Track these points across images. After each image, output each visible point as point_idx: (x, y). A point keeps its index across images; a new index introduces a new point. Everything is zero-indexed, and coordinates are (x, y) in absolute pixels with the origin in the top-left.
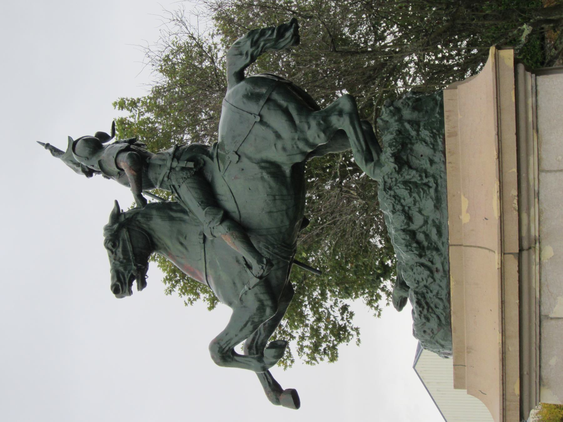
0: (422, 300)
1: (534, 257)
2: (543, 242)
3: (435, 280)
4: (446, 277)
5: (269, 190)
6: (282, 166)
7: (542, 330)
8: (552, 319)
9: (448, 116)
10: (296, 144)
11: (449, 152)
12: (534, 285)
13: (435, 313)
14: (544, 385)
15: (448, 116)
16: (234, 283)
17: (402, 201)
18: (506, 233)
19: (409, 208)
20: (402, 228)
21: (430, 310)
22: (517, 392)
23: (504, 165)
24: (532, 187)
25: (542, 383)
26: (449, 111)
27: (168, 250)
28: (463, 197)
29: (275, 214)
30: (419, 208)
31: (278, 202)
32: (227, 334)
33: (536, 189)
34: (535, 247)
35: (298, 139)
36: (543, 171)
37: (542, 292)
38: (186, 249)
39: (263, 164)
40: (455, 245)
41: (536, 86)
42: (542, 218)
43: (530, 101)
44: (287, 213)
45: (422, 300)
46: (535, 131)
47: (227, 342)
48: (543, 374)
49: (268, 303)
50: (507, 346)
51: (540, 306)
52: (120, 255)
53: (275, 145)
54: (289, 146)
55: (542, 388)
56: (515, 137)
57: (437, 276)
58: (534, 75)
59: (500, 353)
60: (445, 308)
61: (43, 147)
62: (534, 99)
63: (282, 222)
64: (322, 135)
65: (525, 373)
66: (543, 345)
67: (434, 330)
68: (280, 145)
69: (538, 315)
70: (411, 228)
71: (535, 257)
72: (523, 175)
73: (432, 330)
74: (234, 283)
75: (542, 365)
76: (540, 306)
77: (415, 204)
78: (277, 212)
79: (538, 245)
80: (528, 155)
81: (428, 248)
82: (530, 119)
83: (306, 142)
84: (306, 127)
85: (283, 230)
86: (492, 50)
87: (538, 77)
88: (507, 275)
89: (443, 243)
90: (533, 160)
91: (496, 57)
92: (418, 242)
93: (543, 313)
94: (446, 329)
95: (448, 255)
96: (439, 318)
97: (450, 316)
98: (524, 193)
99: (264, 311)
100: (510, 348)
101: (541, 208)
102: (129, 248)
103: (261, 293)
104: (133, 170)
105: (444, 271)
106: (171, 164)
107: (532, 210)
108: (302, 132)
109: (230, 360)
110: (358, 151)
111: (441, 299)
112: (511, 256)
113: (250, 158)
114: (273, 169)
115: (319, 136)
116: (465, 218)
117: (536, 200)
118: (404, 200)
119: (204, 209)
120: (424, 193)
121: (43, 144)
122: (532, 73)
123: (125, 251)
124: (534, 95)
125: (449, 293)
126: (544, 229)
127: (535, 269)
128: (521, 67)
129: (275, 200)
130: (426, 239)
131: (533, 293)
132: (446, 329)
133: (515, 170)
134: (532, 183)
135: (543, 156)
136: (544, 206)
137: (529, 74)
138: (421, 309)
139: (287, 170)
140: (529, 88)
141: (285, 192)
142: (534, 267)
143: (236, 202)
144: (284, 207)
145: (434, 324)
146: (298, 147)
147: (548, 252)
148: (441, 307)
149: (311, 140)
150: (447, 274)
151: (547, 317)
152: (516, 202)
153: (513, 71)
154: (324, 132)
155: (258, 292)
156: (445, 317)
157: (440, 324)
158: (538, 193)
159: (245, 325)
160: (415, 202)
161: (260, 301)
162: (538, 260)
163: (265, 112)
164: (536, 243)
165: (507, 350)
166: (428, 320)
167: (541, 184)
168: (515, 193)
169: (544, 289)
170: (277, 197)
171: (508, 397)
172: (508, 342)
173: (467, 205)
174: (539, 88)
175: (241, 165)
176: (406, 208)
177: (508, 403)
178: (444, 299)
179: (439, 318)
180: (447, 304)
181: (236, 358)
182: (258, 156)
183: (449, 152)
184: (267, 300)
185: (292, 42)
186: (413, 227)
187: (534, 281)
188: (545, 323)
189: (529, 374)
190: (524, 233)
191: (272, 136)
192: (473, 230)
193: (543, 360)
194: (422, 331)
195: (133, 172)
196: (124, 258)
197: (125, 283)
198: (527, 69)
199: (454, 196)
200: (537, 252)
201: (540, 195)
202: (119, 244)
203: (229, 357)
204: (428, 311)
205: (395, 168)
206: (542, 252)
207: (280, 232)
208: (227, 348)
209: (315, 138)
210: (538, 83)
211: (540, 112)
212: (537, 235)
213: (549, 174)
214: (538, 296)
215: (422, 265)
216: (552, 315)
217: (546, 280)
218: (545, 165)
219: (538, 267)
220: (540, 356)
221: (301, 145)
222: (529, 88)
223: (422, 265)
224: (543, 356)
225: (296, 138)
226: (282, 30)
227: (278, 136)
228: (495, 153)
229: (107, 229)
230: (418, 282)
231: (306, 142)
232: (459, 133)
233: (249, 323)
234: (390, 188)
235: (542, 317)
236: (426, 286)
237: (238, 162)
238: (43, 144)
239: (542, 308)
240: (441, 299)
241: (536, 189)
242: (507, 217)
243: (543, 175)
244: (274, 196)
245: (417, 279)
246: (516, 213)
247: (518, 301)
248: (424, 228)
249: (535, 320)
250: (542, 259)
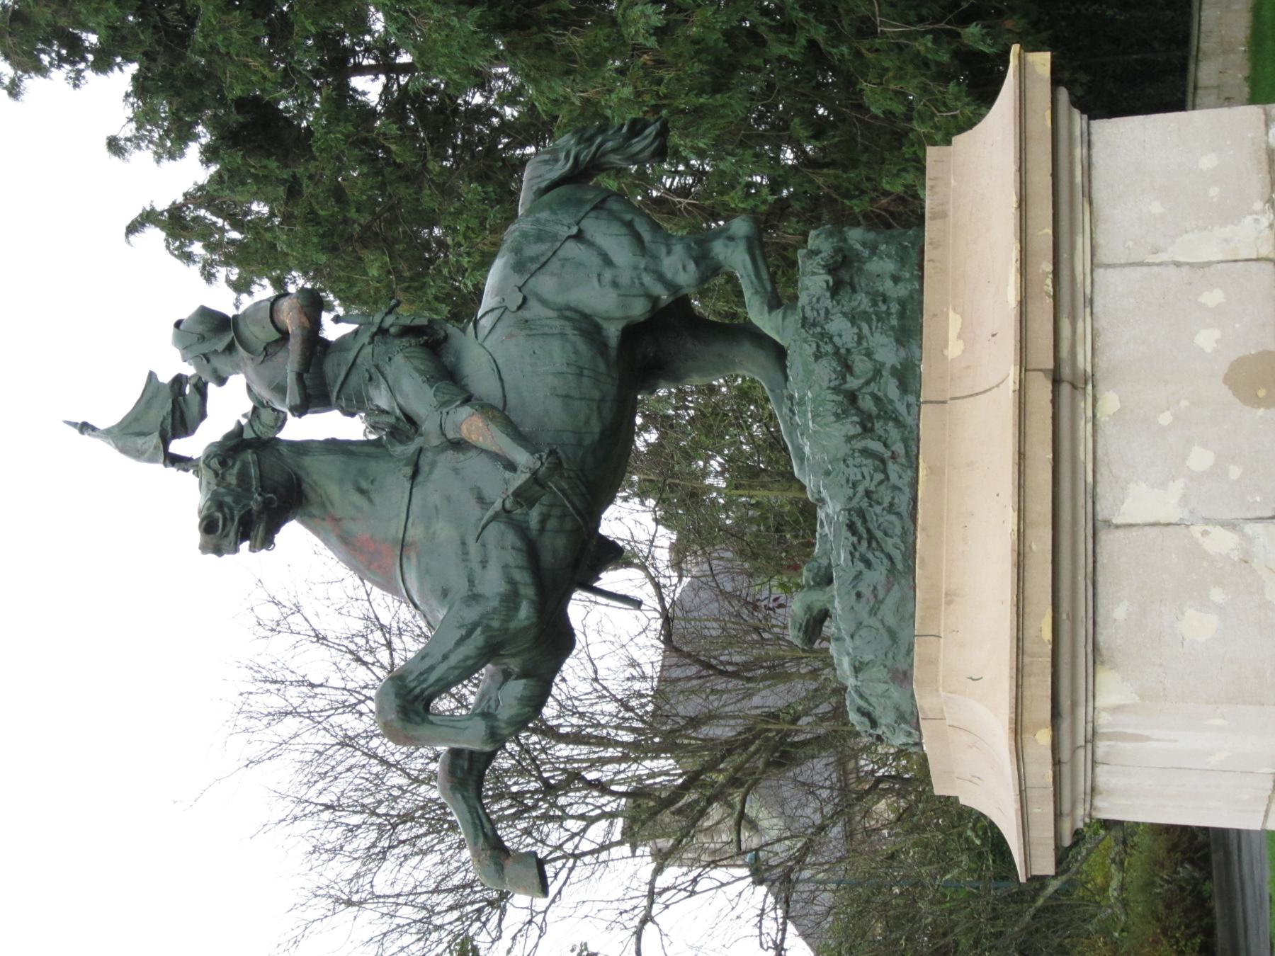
0: (859, 523)
1: (1082, 405)
2: (1100, 386)
3: (887, 478)
4: (911, 467)
5: (573, 357)
6: (605, 325)
7: (1098, 550)
8: (1117, 527)
9: (932, 187)
10: (640, 279)
11: (931, 244)
12: (1082, 457)
13: (882, 551)
14: (1102, 663)
15: (932, 187)
16: (464, 543)
17: (836, 339)
18: (1031, 335)
19: (848, 350)
20: (832, 384)
21: (874, 544)
22: (1047, 634)
23: (1030, 222)
24: (1079, 285)
25: (1098, 659)
26: (935, 179)
27: (328, 504)
28: (951, 313)
29: (577, 403)
30: (867, 349)
31: (586, 381)
32: (423, 658)
33: (1088, 291)
34: (1085, 389)
35: (645, 269)
36: (1100, 266)
37: (1098, 477)
38: (370, 501)
39: (568, 313)
40: (931, 402)
41: (1089, 134)
42: (1098, 344)
43: (1078, 152)
44: (599, 408)
45: (859, 523)
46: (1086, 200)
47: (421, 674)
48: (1101, 639)
49: (528, 591)
50: (1027, 544)
51: (1094, 503)
52: (232, 480)
53: (599, 275)
54: (625, 278)
55: (1098, 667)
56: (1049, 180)
57: (892, 468)
58: (1085, 116)
59: (1013, 550)
60: (905, 532)
61: (76, 431)
62: (1085, 151)
63: (587, 422)
64: (692, 266)
65: (1064, 616)
66: (1100, 579)
67: (879, 587)
68: (608, 275)
69: (1090, 516)
70: (847, 386)
71: (1085, 407)
72: (1064, 256)
73: (875, 588)
74: (464, 543)
75: (1099, 619)
76: (1094, 503)
77: (859, 342)
78: (581, 399)
79: (1090, 387)
80: (1072, 233)
81: (879, 417)
82: (1078, 179)
83: (660, 277)
84: (663, 250)
85: (587, 441)
86: (1015, 49)
87: (1092, 122)
88: (1030, 408)
89: (909, 406)
90: (1082, 244)
91: (1021, 59)
92: (860, 411)
93: (1100, 517)
94: (903, 581)
95: (918, 426)
96: (890, 558)
97: (915, 552)
98: (1065, 273)
99: (516, 608)
100: (1034, 547)
101: (1096, 326)
102: (253, 472)
103: (517, 567)
104: (305, 314)
105: (907, 454)
106: (382, 321)
107: (1080, 325)
108: (655, 258)
109: (418, 719)
110: (757, 292)
111: (898, 514)
112: (1041, 374)
113: (544, 302)
114: (588, 326)
115: (684, 268)
116: (955, 349)
117: (1088, 310)
118: (840, 336)
119: (431, 387)
120: (878, 321)
121: (74, 425)
122: (1083, 112)
123: (243, 476)
124: (1085, 145)
125: (914, 500)
126: (1102, 363)
127: (1085, 429)
128: (1063, 94)
129: (581, 375)
130: (876, 405)
131: (1081, 471)
132: (903, 581)
133: (1049, 231)
134: (1079, 279)
135: (1101, 240)
136: (1102, 323)
137: (1076, 113)
138: (855, 539)
139: (613, 332)
140: (1078, 133)
141: (602, 367)
142: (1082, 423)
143: (501, 379)
144: (596, 394)
145: (878, 575)
146: (642, 284)
147: (1110, 402)
148: (898, 531)
149: (669, 275)
150: (912, 463)
151: (1108, 524)
152: (1049, 282)
153: (1052, 798)
154: (697, 261)
155: (512, 563)
156: (904, 555)
157: (892, 570)
158: (1091, 301)
159: (469, 633)
160: (860, 338)
161: (512, 582)
162: (1090, 413)
163: (586, 224)
164: (1086, 383)
165: (1027, 549)
166: (868, 564)
167: (1096, 287)
168: (1049, 268)
169: (1103, 470)
170: (586, 372)
171: (1029, 646)
172: (1031, 534)
173: (958, 327)
174: (1094, 138)
175: (525, 314)
176: (843, 351)
177: (1027, 660)
178: (905, 514)
179: (890, 558)
180: (909, 524)
181: (431, 717)
182: (561, 299)
183: (931, 244)
184: (526, 584)
185: (652, 148)
186: (853, 383)
187: (1082, 448)
188: (1103, 536)
189: (1073, 619)
190: (1065, 352)
191: (594, 260)
192: (968, 367)
193: (1101, 611)
194: (853, 593)
195: (304, 320)
196: (238, 485)
197: (232, 519)
198: (1076, 103)
199: (935, 315)
200: (1090, 400)
201: (1095, 305)
202: (234, 465)
203: (418, 714)
204: (869, 543)
205: (827, 282)
206: (1099, 404)
207: (580, 444)
208: (418, 690)
209: (677, 272)
210: (1093, 130)
211: (1094, 173)
212: (1089, 369)
213: (1110, 271)
214: (1090, 479)
215: (865, 452)
216: (1116, 521)
217: (1106, 454)
218: (1103, 256)
219: (1090, 426)
220: (1095, 562)
221: (647, 279)
222: (1078, 133)
223: (865, 452)
224: (1102, 602)
225: (642, 266)
226: (639, 127)
227: (607, 261)
228: (1013, 200)
229: (212, 444)
230: (854, 485)
231: (660, 277)
232: (951, 214)
233: (479, 630)
234: (814, 325)
235: (1099, 524)
236: (868, 494)
237: (519, 308)
238: (74, 425)
239: (1098, 507)
240: (898, 514)
241: (1088, 291)
242: (1032, 308)
243: (1099, 273)
244: (581, 368)
245: (852, 478)
246: (1049, 301)
247: (1050, 456)
248: (873, 387)
249: (1084, 531)
250: (1098, 416)
